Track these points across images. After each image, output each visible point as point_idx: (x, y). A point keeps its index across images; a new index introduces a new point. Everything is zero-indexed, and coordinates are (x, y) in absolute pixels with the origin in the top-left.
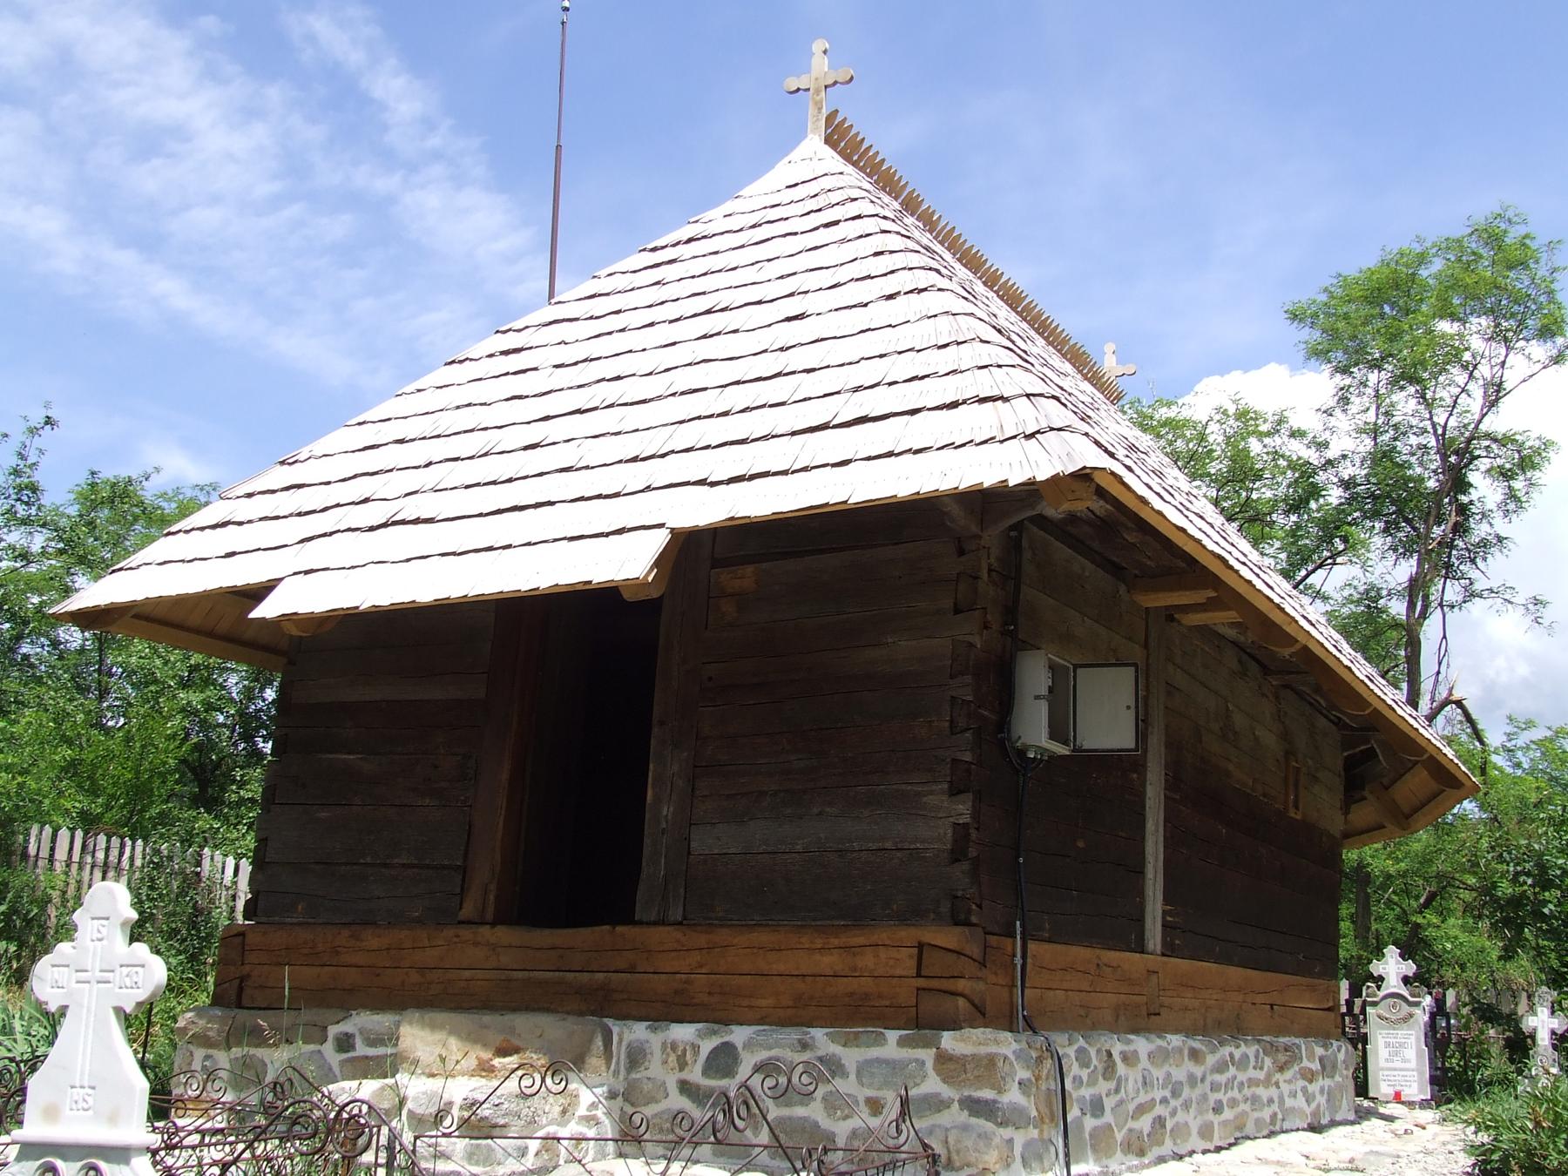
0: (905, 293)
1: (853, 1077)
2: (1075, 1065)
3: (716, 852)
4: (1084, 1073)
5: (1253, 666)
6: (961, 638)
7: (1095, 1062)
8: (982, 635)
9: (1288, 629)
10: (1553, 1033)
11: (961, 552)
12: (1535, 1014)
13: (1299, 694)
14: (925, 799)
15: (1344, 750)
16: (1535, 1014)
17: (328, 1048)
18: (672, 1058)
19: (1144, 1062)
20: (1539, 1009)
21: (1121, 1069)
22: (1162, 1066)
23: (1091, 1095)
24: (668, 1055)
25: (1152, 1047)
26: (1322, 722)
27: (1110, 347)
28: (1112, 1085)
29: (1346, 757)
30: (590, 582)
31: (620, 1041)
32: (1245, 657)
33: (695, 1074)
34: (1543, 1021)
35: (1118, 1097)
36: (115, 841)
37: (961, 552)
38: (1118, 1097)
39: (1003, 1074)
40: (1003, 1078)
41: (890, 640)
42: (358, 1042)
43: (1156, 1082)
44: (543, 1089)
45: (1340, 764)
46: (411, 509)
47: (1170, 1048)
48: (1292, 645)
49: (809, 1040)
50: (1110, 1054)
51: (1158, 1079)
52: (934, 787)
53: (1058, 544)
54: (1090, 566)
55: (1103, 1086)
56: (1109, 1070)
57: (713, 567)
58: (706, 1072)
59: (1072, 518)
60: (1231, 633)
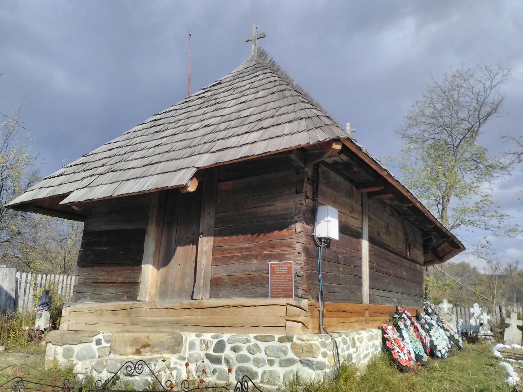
0: (278, 92)
1: (264, 352)
2: (342, 344)
3: (220, 275)
4: (345, 347)
5: (395, 212)
6: (298, 202)
7: (348, 342)
8: (305, 201)
9: (409, 198)
10: (488, 320)
11: (298, 173)
12: (483, 315)
13: (410, 221)
14: (287, 256)
15: (423, 238)
16: (483, 315)
17: (93, 345)
18: (204, 346)
19: (365, 340)
20: (484, 313)
21: (358, 344)
22: (371, 341)
23: (348, 354)
24: (202, 344)
25: (368, 335)
26: (416, 229)
27: (348, 124)
28: (355, 349)
29: (424, 240)
30: (168, 187)
31: (186, 340)
32: (393, 210)
33: (211, 352)
34: (485, 317)
35: (357, 353)
36: (65, 276)
37: (298, 173)
38: (357, 353)
39: (315, 351)
40: (316, 353)
41: (275, 204)
42: (103, 341)
43: (369, 346)
44: (135, 371)
45: (422, 242)
46: (116, 167)
47: (374, 334)
48: (410, 204)
49: (249, 339)
50: (353, 339)
51: (370, 345)
52: (290, 252)
53: (331, 172)
54: (342, 180)
55: (351, 350)
56: (354, 345)
57: (219, 182)
58: (215, 351)
59: (336, 163)
60: (388, 202)
